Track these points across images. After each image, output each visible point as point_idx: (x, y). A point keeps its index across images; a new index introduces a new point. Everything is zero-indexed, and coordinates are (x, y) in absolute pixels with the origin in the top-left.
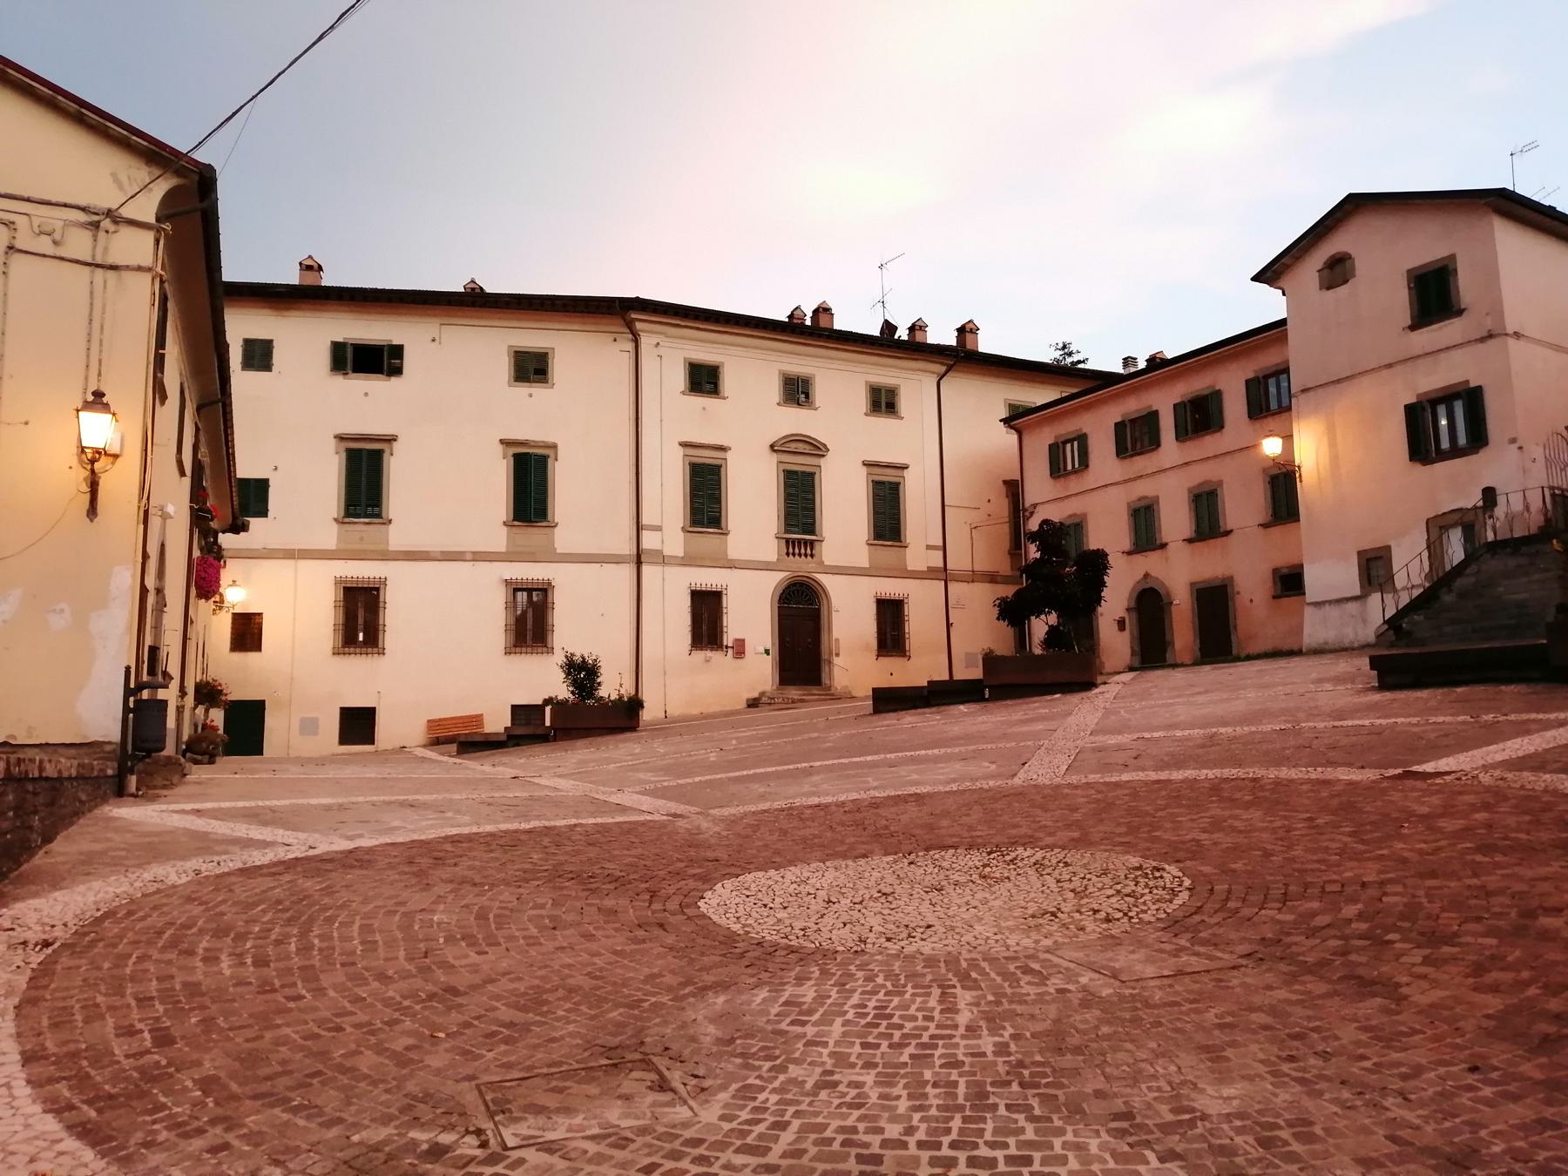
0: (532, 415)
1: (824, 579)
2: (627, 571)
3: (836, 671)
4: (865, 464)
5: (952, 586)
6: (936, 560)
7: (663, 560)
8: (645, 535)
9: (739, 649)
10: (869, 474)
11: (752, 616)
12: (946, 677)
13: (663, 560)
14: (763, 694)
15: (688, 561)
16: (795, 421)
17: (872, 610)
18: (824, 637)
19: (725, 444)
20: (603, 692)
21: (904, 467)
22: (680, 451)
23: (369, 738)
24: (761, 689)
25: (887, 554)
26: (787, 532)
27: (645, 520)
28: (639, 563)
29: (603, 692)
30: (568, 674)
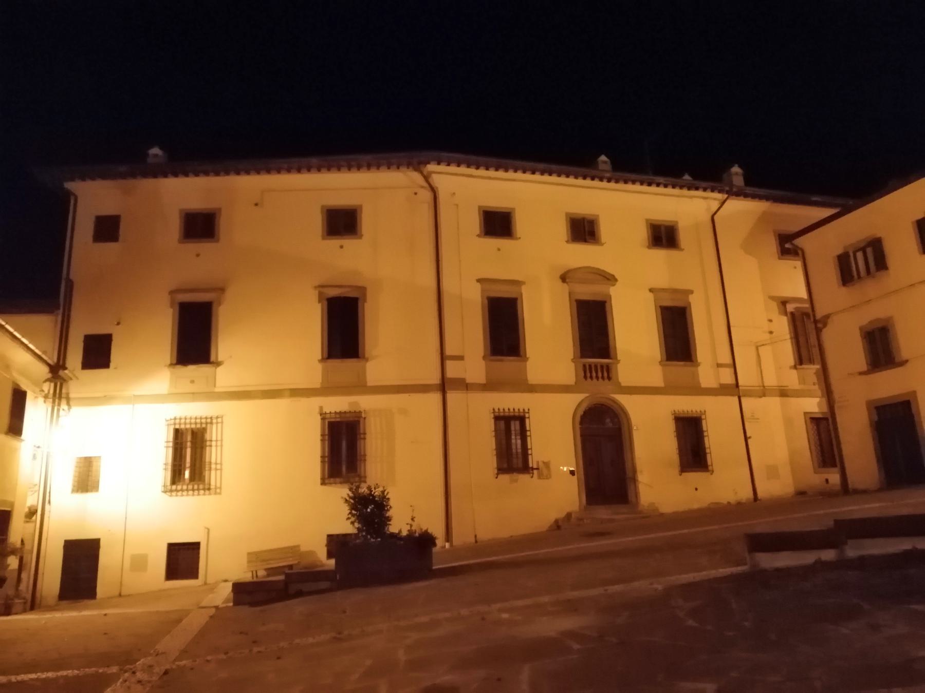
0: (348, 260)
1: (625, 400)
2: (436, 397)
3: (642, 489)
4: (479, 281)
5: (747, 402)
6: (727, 377)
7: (463, 385)
8: (449, 364)
9: (544, 471)
10: (483, 291)
11: (554, 438)
12: (746, 494)
13: (463, 385)
14: (569, 516)
15: (490, 386)
16: (582, 255)
17: (670, 428)
18: (627, 456)
19: (520, 279)
20: (393, 528)
21: (692, 292)
22: (651, 296)
23: (193, 573)
24: (568, 510)
25: (679, 369)
26: (583, 355)
27: (449, 351)
28: (772, 343)
29: (393, 528)
30: (353, 507)
